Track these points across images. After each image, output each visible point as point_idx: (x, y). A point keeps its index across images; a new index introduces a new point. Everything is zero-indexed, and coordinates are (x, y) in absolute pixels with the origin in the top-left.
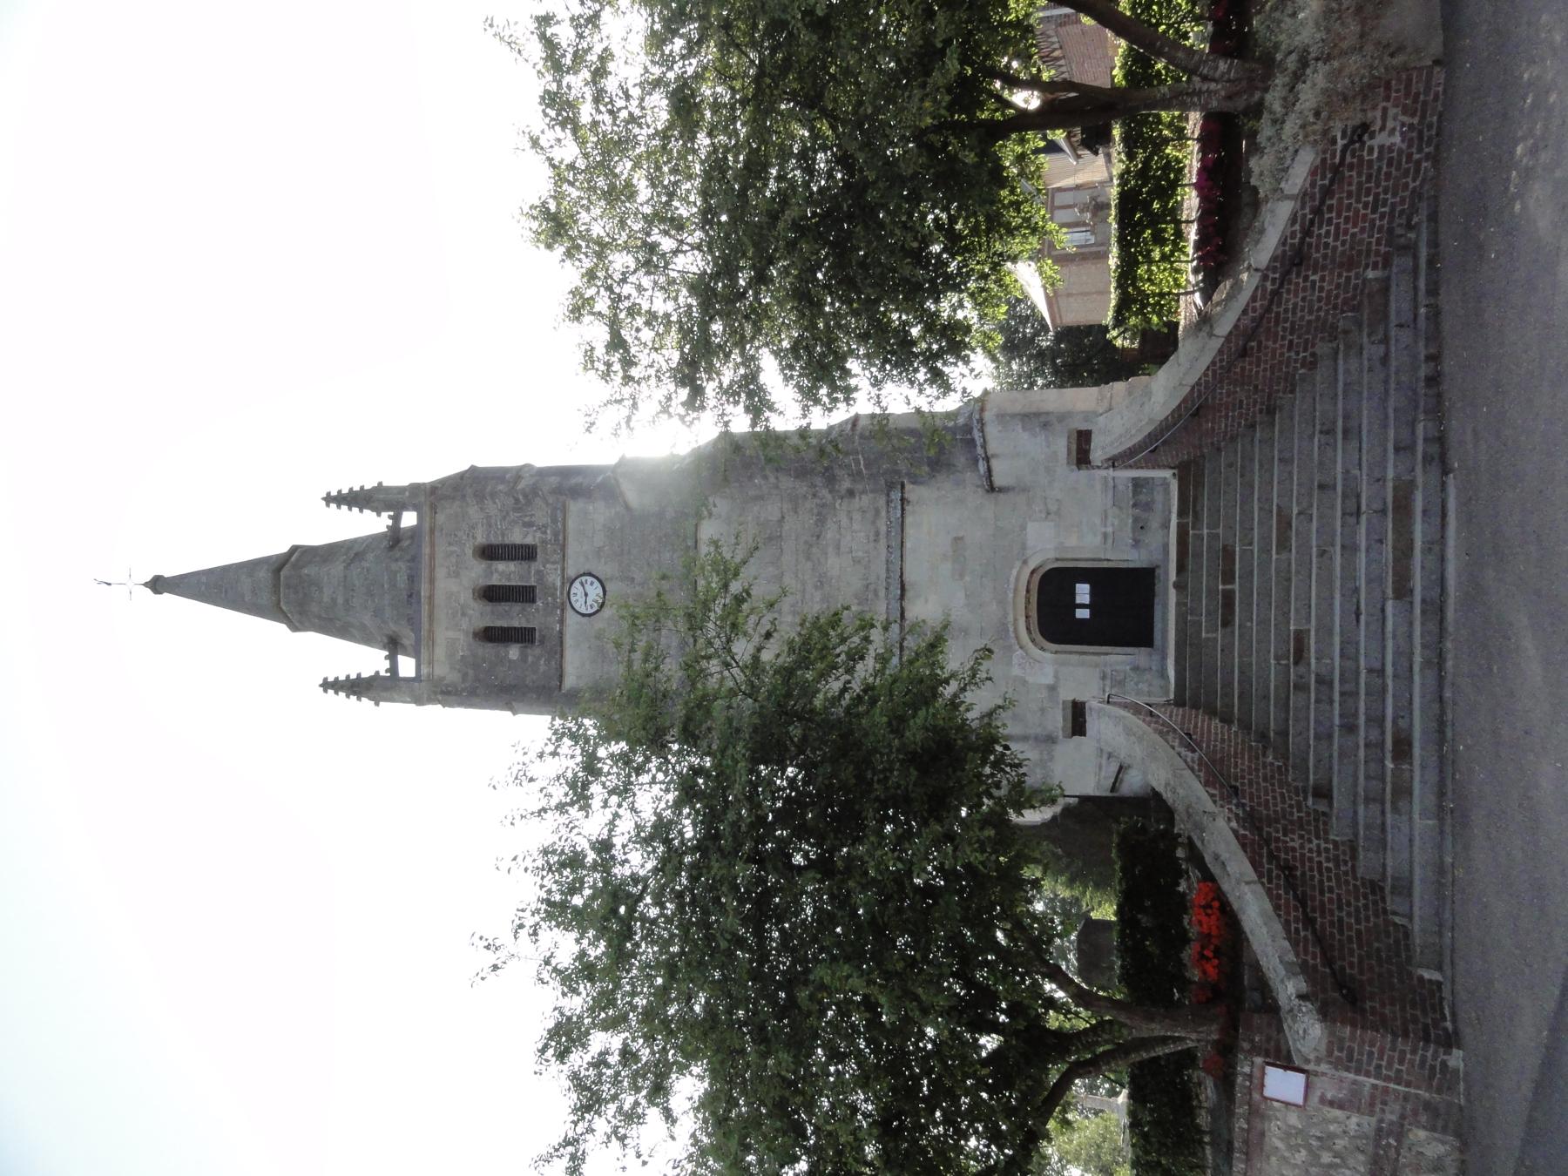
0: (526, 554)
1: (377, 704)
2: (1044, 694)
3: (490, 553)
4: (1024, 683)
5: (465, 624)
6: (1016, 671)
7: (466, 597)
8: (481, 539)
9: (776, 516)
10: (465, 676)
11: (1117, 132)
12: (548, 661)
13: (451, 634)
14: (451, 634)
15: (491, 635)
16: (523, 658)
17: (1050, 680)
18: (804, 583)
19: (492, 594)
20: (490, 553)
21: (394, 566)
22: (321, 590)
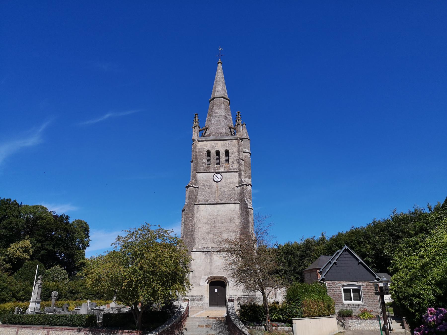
0: (227, 162)
1: (88, 246)
2: (198, 283)
3: (227, 152)
4: (200, 279)
5: (211, 148)
6: (203, 277)
7: (217, 148)
8: (230, 151)
9: (235, 222)
10: (199, 149)
11: (220, 88)
12: (203, 169)
13: (208, 145)
14: (208, 145)
15: (209, 153)
16: (204, 163)
17: (201, 284)
18: (221, 228)
19: (218, 153)
20: (227, 152)
21: (224, 128)
22: (218, 109)
